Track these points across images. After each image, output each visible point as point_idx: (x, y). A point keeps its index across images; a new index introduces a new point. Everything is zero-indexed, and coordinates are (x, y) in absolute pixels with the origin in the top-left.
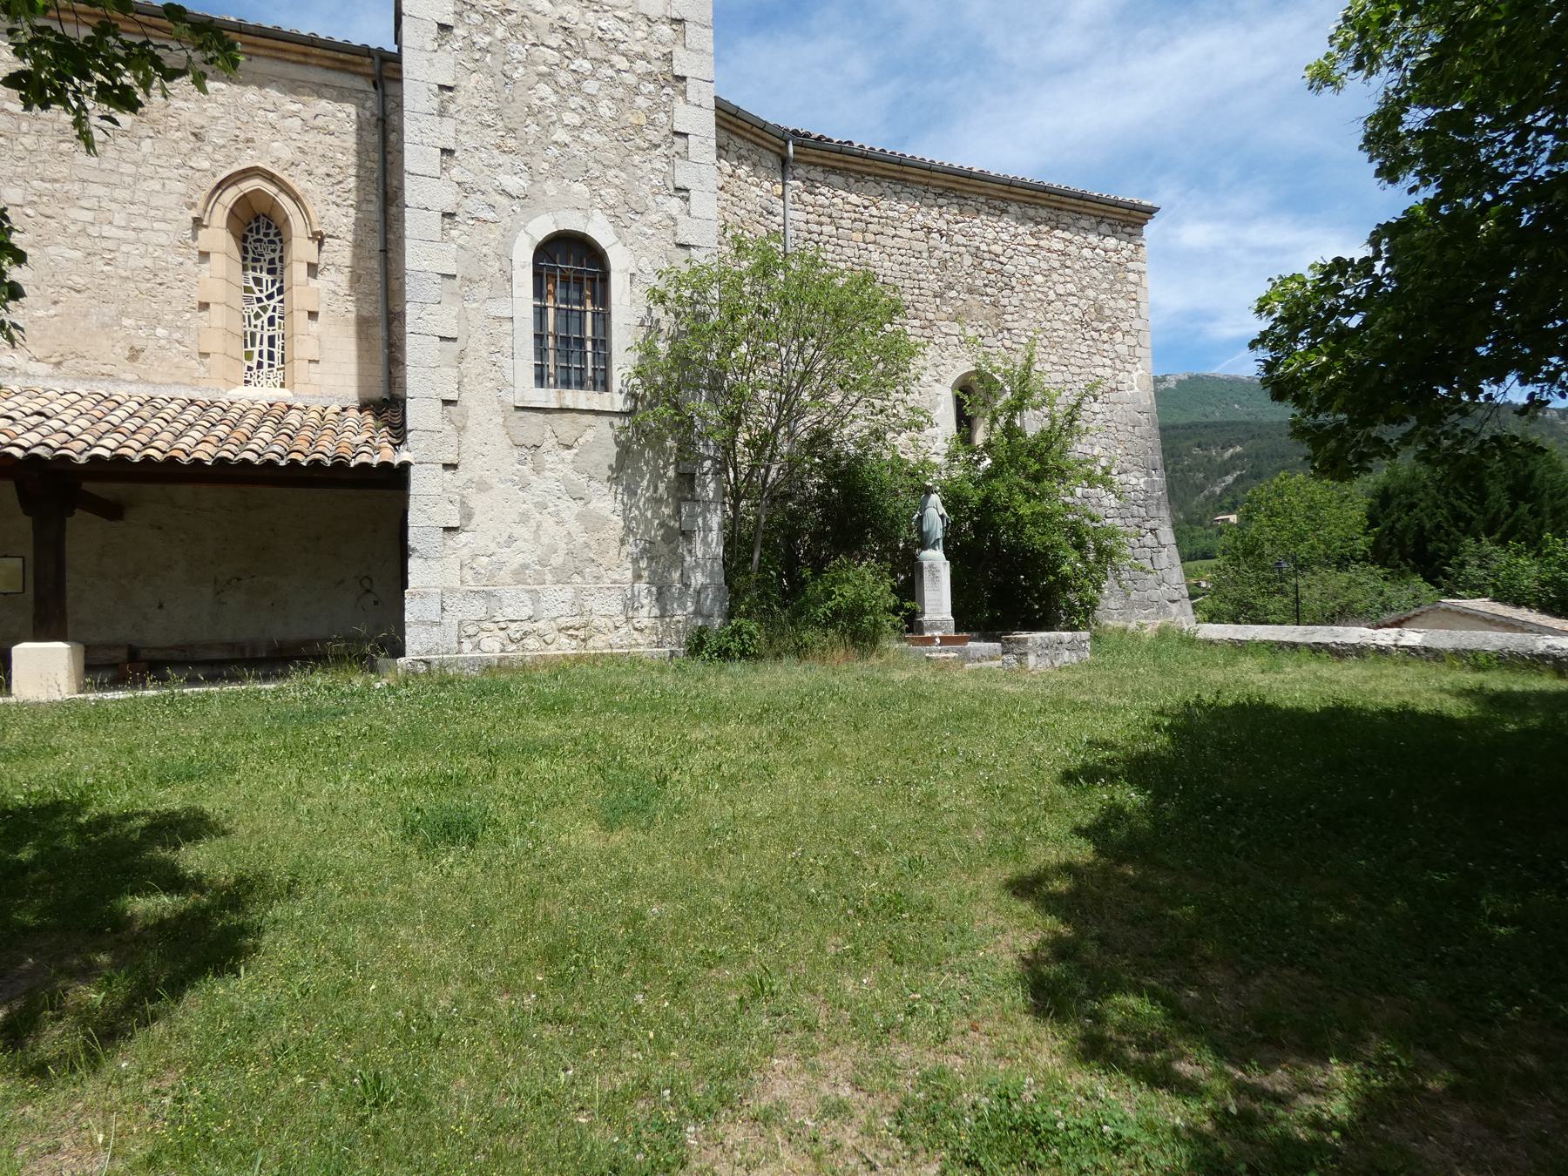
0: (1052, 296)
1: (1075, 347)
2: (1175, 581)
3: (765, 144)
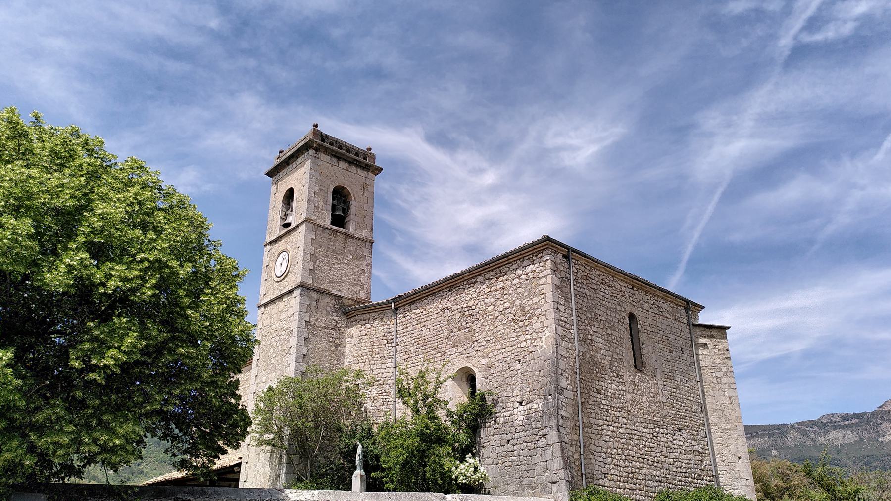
0: (497, 313)
1: (509, 336)
2: (555, 468)
3: (384, 309)
